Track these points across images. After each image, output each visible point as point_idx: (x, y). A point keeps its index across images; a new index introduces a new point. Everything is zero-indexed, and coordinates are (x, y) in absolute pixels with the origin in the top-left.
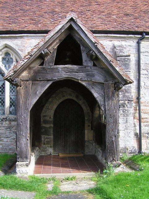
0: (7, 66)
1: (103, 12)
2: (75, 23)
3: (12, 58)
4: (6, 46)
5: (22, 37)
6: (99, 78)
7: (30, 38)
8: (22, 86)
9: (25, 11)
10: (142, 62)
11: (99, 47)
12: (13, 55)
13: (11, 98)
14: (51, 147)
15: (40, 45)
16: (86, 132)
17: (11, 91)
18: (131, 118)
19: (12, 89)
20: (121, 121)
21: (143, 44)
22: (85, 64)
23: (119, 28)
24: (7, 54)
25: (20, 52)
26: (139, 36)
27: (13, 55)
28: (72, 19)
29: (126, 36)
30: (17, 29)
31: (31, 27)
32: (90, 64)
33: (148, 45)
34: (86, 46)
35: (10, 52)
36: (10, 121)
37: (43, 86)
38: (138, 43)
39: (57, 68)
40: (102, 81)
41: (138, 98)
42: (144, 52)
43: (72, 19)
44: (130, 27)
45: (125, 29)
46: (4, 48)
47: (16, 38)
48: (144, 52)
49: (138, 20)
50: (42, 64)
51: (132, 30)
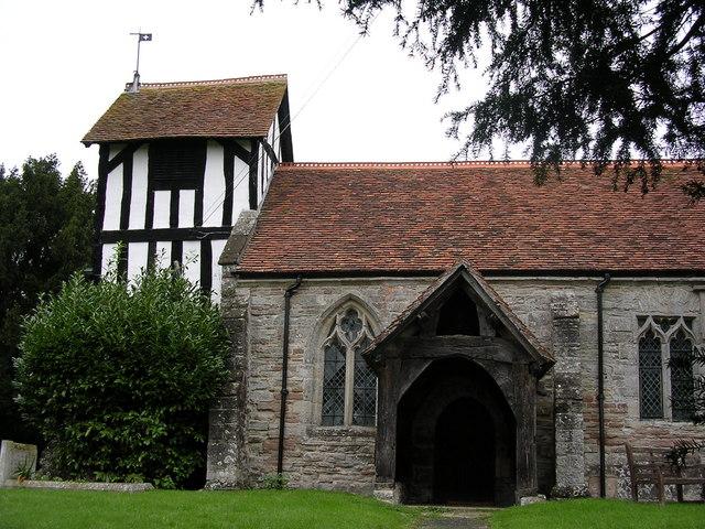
0: (351, 334)
1: (536, 229)
2: (468, 272)
3: (360, 321)
4: (350, 298)
5: (379, 282)
6: (504, 355)
7: (395, 284)
8: (543, 188)
9: (384, 230)
10: (606, 327)
11: (503, 308)
12: (362, 313)
13: (355, 395)
14: (429, 487)
15: (416, 306)
16: (498, 461)
17: (356, 381)
18: (579, 433)
19: (359, 378)
20: (559, 437)
21: (609, 293)
22: (483, 334)
23: (562, 265)
24: (351, 312)
25: (376, 310)
26: (601, 279)
27: (362, 313)
28: (462, 267)
29: (573, 279)
30: (371, 265)
31: (399, 264)
32: (491, 334)
33: (702, 287)
34: (485, 307)
35: (358, 308)
36: (355, 435)
37: (418, 367)
38: (599, 292)
39: (440, 340)
40: (510, 360)
41: (600, 397)
42: (609, 309)
43: (462, 267)
44: (582, 262)
45: (573, 266)
46: (346, 302)
47: (369, 283)
48: (609, 309)
49: (602, 246)
50: (417, 334)
51: (585, 267)
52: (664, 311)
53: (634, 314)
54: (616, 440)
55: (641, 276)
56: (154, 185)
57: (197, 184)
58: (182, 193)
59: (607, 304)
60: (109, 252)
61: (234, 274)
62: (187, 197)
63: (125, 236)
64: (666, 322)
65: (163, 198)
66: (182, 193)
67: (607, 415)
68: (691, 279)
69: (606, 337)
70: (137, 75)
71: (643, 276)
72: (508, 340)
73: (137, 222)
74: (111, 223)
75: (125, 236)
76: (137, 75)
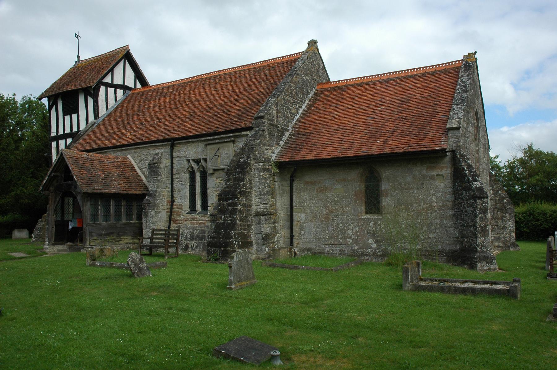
10: (175, 166)
42: (176, 157)
52: (195, 157)
53: (185, 159)
54: (179, 222)
55: (210, 136)
56: (65, 114)
57: (77, 111)
58: (73, 115)
59: (175, 155)
60: (54, 144)
61: (271, 125)
62: (74, 116)
63: (57, 138)
64: (197, 161)
65: (67, 118)
66: (73, 115)
67: (175, 209)
68: (203, 139)
69: (175, 171)
70: (78, 57)
71: (186, 139)
72: (212, 174)
73: (61, 132)
74: (53, 133)
75: (57, 138)
76: (78, 57)
